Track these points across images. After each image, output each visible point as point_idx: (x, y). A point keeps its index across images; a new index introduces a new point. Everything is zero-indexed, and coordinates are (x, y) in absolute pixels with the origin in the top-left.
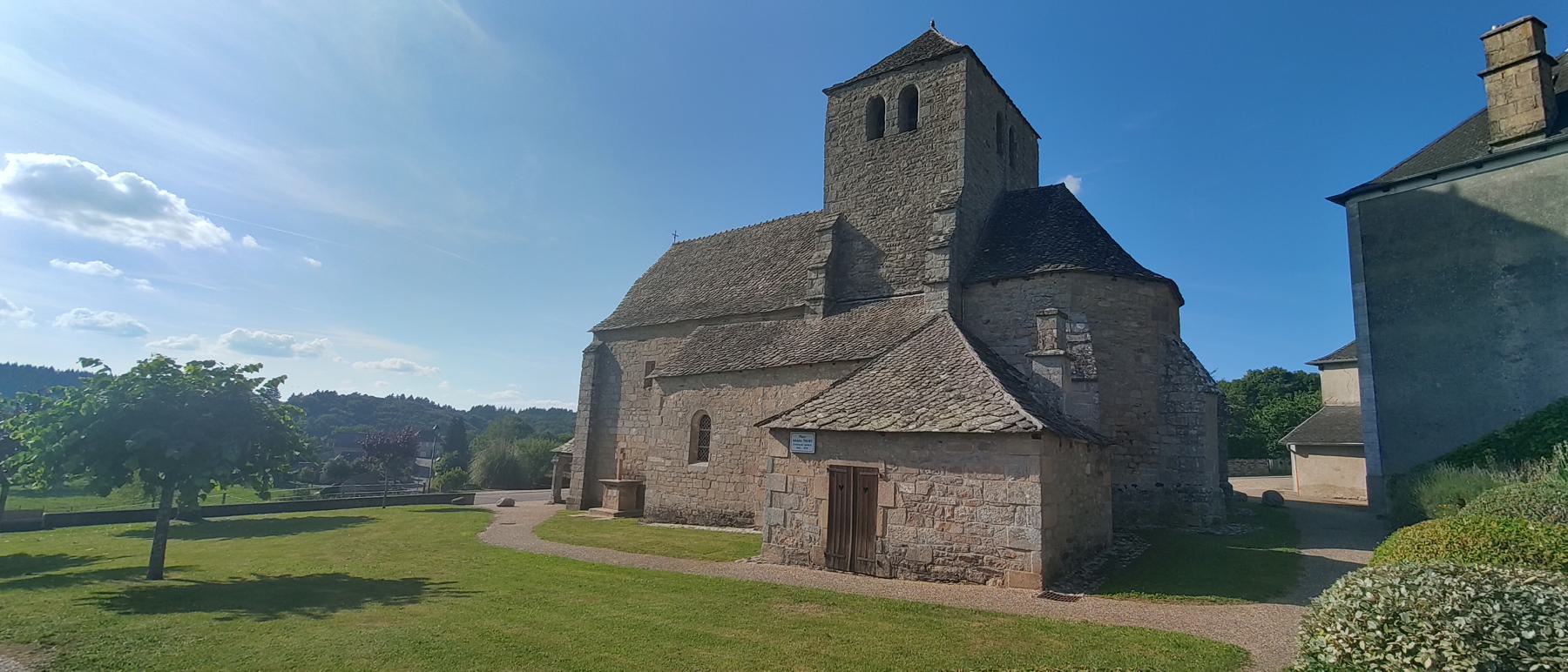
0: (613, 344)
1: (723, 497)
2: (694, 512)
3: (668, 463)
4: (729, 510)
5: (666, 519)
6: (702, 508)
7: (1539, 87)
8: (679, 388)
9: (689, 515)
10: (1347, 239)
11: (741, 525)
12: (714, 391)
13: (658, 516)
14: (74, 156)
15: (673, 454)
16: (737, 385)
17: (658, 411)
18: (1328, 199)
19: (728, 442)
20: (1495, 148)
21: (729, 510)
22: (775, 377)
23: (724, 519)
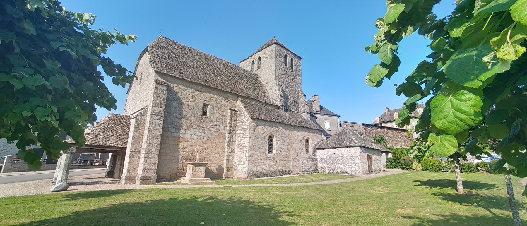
0: (174, 85)
1: (280, 166)
2: (271, 172)
3: (259, 153)
4: (283, 170)
5: (259, 176)
6: (274, 170)
7: (161, 122)
8: (263, 125)
9: (269, 173)
10: (401, 41)
11: (287, 174)
12: (277, 129)
13: (256, 175)
14: (466, 203)
15: (260, 150)
16: (284, 128)
17: (253, 132)
18: (427, 57)
19: (282, 147)
20: (373, 192)
21: (283, 170)
22: (295, 129)
23: (282, 173)
